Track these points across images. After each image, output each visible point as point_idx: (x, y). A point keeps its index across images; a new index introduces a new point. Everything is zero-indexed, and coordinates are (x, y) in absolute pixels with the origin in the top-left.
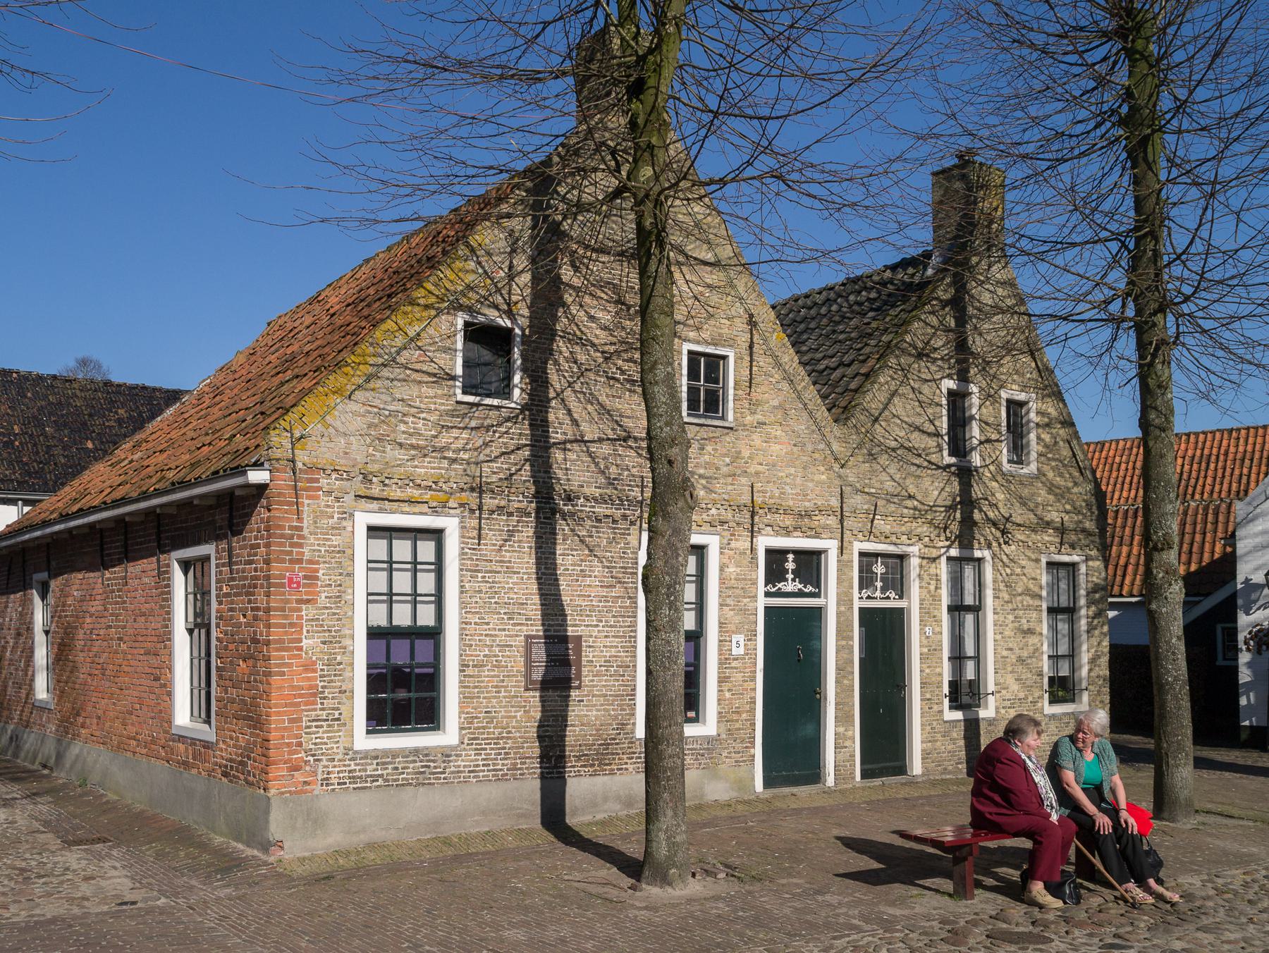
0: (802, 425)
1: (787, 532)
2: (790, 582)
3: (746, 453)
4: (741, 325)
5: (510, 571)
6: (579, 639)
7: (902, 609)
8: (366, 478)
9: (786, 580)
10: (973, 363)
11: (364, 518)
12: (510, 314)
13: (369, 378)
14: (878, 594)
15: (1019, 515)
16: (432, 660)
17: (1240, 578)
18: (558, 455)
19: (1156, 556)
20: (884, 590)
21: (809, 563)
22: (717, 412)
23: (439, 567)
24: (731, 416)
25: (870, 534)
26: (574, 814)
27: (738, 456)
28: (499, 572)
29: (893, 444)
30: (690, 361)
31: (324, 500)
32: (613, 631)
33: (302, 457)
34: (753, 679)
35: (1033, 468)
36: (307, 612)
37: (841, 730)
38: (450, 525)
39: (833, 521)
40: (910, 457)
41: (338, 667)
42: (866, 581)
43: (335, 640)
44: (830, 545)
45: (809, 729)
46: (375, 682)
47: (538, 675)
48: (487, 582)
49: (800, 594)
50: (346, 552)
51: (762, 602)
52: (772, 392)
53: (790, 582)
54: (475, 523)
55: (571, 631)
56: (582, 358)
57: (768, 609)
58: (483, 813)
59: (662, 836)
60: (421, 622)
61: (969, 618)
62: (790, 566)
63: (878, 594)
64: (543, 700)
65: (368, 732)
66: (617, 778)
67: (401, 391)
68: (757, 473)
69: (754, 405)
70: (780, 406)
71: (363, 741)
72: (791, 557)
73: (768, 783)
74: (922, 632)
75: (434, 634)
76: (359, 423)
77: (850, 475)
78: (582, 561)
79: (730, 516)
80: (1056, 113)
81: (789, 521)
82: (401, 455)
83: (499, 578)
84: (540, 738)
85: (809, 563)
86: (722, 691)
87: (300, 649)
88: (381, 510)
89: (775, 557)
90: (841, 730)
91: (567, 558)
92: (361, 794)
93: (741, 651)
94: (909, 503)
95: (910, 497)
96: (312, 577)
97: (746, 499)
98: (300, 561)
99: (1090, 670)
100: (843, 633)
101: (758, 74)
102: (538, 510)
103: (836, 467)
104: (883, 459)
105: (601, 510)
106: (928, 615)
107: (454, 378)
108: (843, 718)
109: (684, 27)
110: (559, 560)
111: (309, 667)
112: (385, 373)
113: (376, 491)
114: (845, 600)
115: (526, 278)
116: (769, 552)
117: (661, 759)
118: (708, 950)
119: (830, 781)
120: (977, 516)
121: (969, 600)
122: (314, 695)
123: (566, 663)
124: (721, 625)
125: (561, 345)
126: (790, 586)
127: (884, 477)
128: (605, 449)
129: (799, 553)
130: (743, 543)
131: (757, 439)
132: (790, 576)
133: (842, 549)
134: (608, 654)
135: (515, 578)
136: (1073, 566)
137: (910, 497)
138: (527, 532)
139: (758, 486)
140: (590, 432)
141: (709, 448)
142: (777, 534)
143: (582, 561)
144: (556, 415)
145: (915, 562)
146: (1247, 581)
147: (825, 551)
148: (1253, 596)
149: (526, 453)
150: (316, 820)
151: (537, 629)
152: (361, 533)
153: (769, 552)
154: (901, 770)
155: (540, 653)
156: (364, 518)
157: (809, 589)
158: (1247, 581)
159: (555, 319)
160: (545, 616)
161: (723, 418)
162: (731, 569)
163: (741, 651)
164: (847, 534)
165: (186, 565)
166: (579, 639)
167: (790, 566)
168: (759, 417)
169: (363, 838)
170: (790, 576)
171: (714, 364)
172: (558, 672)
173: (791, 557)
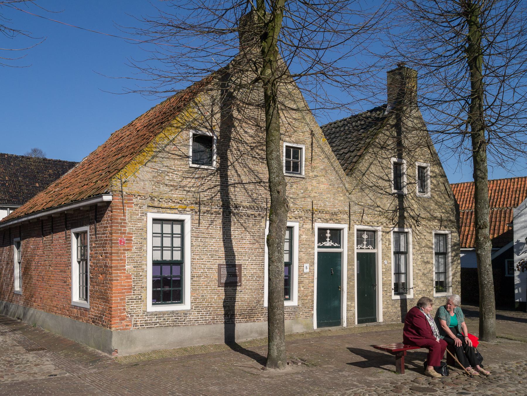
0: (333, 177)
1: (327, 221)
2: (328, 242)
3: (310, 188)
4: (308, 135)
5: (212, 237)
6: (240, 266)
7: (375, 253)
8: (152, 199)
9: (327, 241)
10: (404, 151)
11: (151, 215)
12: (212, 130)
13: (153, 157)
14: (365, 247)
15: (423, 214)
16: (179, 274)
17: (515, 240)
18: (232, 189)
19: (480, 231)
20: (367, 245)
21: (336, 234)
22: (298, 171)
23: (182, 236)
24: (303, 173)
25: (361, 222)
26: (238, 338)
27: (306, 189)
28: (207, 238)
29: (371, 185)
30: (287, 150)
31: (135, 208)
32: (255, 262)
33: (125, 190)
34: (313, 282)
35: (429, 194)
36: (128, 254)
37: (349, 303)
38: (187, 218)
39: (346, 217)
40: (378, 190)
41: (140, 277)
42: (360, 241)
43: (139, 266)
44: (345, 226)
45: (336, 303)
46: (156, 283)
47: (223, 280)
48: (202, 242)
49: (332, 247)
50: (144, 229)
51: (316, 250)
52: (321, 163)
53: (328, 242)
54: (197, 217)
55: (237, 262)
56: (242, 149)
57: (319, 253)
58: (201, 338)
59: (275, 347)
60: (175, 258)
61: (403, 257)
62: (328, 235)
63: (365, 247)
64: (226, 291)
65: (153, 304)
66: (256, 323)
67: (167, 163)
68: (314, 197)
69: (313, 168)
70: (324, 169)
71: (151, 308)
72: (328, 231)
73: (319, 325)
74: (383, 263)
75: (180, 264)
76: (149, 176)
77: (353, 197)
78: (242, 233)
79: (303, 214)
80: (439, 47)
81: (328, 217)
82: (167, 189)
83: (207, 240)
84: (224, 307)
85: (336, 234)
86: (300, 287)
87: (125, 270)
88: (158, 212)
89: (322, 231)
90: (349, 303)
91: (235, 232)
92: (150, 330)
93: (308, 270)
94: (378, 209)
95: (378, 206)
96: (130, 240)
97: (310, 207)
98: (124, 233)
99: (453, 279)
100: (350, 263)
101: (315, 31)
102: (223, 212)
103: (347, 194)
104: (367, 191)
105: (249, 212)
106: (385, 255)
107: (188, 157)
108: (350, 298)
109: (284, 11)
110: (232, 233)
111: (128, 277)
112: (160, 155)
113: (156, 204)
114: (351, 249)
115: (218, 116)
116: (320, 229)
117: (274, 316)
118: (294, 395)
119: (345, 324)
120: (406, 214)
121: (402, 249)
122: (131, 289)
123: (235, 275)
124: (300, 260)
125: (233, 143)
126: (328, 243)
127: (367, 198)
128: (251, 187)
129: (332, 230)
130: (308, 226)
131: (314, 183)
132: (328, 239)
133: (349, 228)
134: (253, 272)
135: (214, 240)
136: (446, 235)
137: (378, 206)
138: (219, 221)
139: (315, 202)
140: (245, 179)
141: (294, 186)
142: (323, 222)
143: (242, 233)
144: (231, 172)
145: (380, 233)
146: (518, 241)
147: (343, 229)
148: (521, 248)
149: (219, 188)
150: (131, 341)
151: (223, 261)
152: (150, 222)
153: (320, 229)
154: (374, 320)
155: (224, 272)
156: (151, 215)
157: (336, 245)
158: (518, 241)
159: (231, 132)
160: (226, 256)
161: (300, 174)
162: (304, 236)
163: (308, 270)
164: (352, 222)
165: (77, 235)
166: (240, 266)
167: (328, 235)
168: (315, 173)
169: (151, 348)
170: (328, 239)
171: (297, 151)
172: (232, 279)
173: (328, 231)
